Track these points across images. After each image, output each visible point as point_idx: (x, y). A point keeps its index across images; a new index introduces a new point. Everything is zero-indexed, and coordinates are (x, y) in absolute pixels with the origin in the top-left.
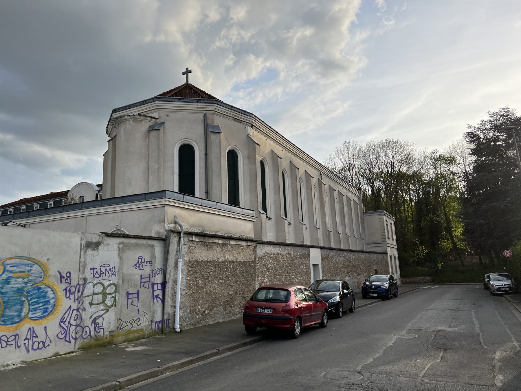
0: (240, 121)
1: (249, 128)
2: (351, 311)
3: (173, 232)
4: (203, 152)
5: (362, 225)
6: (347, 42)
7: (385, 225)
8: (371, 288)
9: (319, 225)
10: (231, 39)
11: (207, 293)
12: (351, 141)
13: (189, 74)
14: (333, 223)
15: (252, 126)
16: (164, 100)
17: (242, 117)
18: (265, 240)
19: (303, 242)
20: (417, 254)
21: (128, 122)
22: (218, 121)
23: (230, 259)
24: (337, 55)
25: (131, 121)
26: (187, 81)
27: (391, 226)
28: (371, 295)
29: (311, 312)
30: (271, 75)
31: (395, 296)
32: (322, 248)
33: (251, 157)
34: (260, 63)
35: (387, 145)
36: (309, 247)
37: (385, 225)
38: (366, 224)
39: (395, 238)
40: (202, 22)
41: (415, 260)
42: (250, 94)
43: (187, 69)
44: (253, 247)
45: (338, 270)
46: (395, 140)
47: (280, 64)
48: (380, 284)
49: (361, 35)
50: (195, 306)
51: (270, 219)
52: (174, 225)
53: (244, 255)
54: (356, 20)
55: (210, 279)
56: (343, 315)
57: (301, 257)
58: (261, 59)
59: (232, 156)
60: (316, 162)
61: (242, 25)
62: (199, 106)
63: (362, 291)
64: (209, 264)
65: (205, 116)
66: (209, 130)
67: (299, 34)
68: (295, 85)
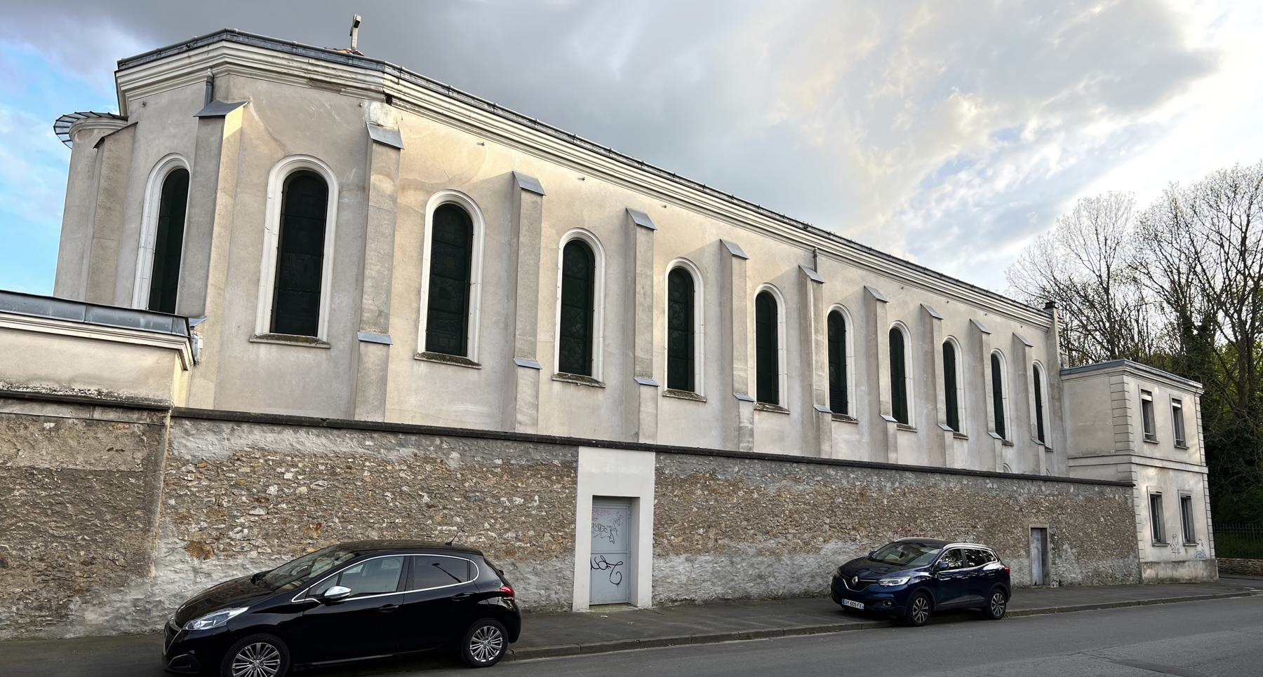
5: (1052, 407)
36: (573, 443)
38: (1067, 403)
62: (193, 59)
65: (211, 82)
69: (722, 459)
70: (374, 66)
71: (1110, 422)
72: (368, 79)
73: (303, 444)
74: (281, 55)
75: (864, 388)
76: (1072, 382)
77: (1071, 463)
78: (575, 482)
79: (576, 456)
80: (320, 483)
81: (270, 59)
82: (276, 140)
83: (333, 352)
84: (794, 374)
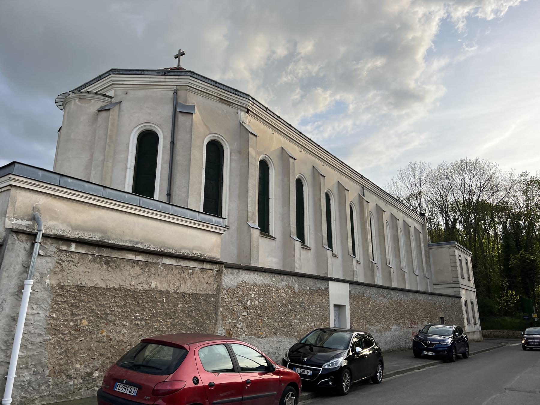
0: (229, 103)
1: (243, 113)
2: (375, 381)
3: (17, 232)
4: (169, 140)
5: (426, 260)
6: (422, 71)
7: (458, 261)
8: (426, 344)
9: (392, 264)
10: (298, 73)
11: (100, 341)
12: (418, 163)
13: (182, 57)
14: (381, 254)
15: (248, 111)
16: (121, 72)
17: (230, 96)
18: (253, 264)
19: (327, 273)
20: (504, 300)
21: (73, 102)
22: (193, 99)
23: (163, 287)
24: (412, 85)
25: (77, 100)
26: (179, 65)
27: (467, 263)
28: (426, 353)
29: (241, 394)
30: (339, 109)
31: (465, 356)
32: (351, 283)
33: (243, 153)
34: (328, 95)
35: (464, 166)
37: (458, 261)
38: (431, 259)
39: (472, 278)
40: (269, 58)
41: (501, 308)
42: (318, 127)
43: (180, 50)
44: (215, 273)
45: (380, 316)
46: (473, 159)
47: (349, 97)
48: (439, 338)
49: (438, 64)
50: (66, 364)
51: (308, 248)
52: (30, 223)
53: (197, 283)
54: (433, 47)
55: (111, 318)
56: (350, 391)
57: (312, 293)
58: (329, 92)
59: (215, 150)
60: (356, 173)
61: (309, 59)
63: (414, 346)
64: (109, 293)
65: (175, 92)
66: (180, 110)
67: (369, 65)
68: (366, 117)
69: (365, 287)
70: (245, 96)
71: (450, 269)
72: (243, 102)
73: (256, 280)
74: (211, 86)
75: (379, 251)
76: (433, 250)
77: (435, 287)
78: (329, 299)
79: (328, 285)
80: (261, 299)
81: (206, 87)
82: (206, 126)
83: (230, 231)
84: (360, 244)
